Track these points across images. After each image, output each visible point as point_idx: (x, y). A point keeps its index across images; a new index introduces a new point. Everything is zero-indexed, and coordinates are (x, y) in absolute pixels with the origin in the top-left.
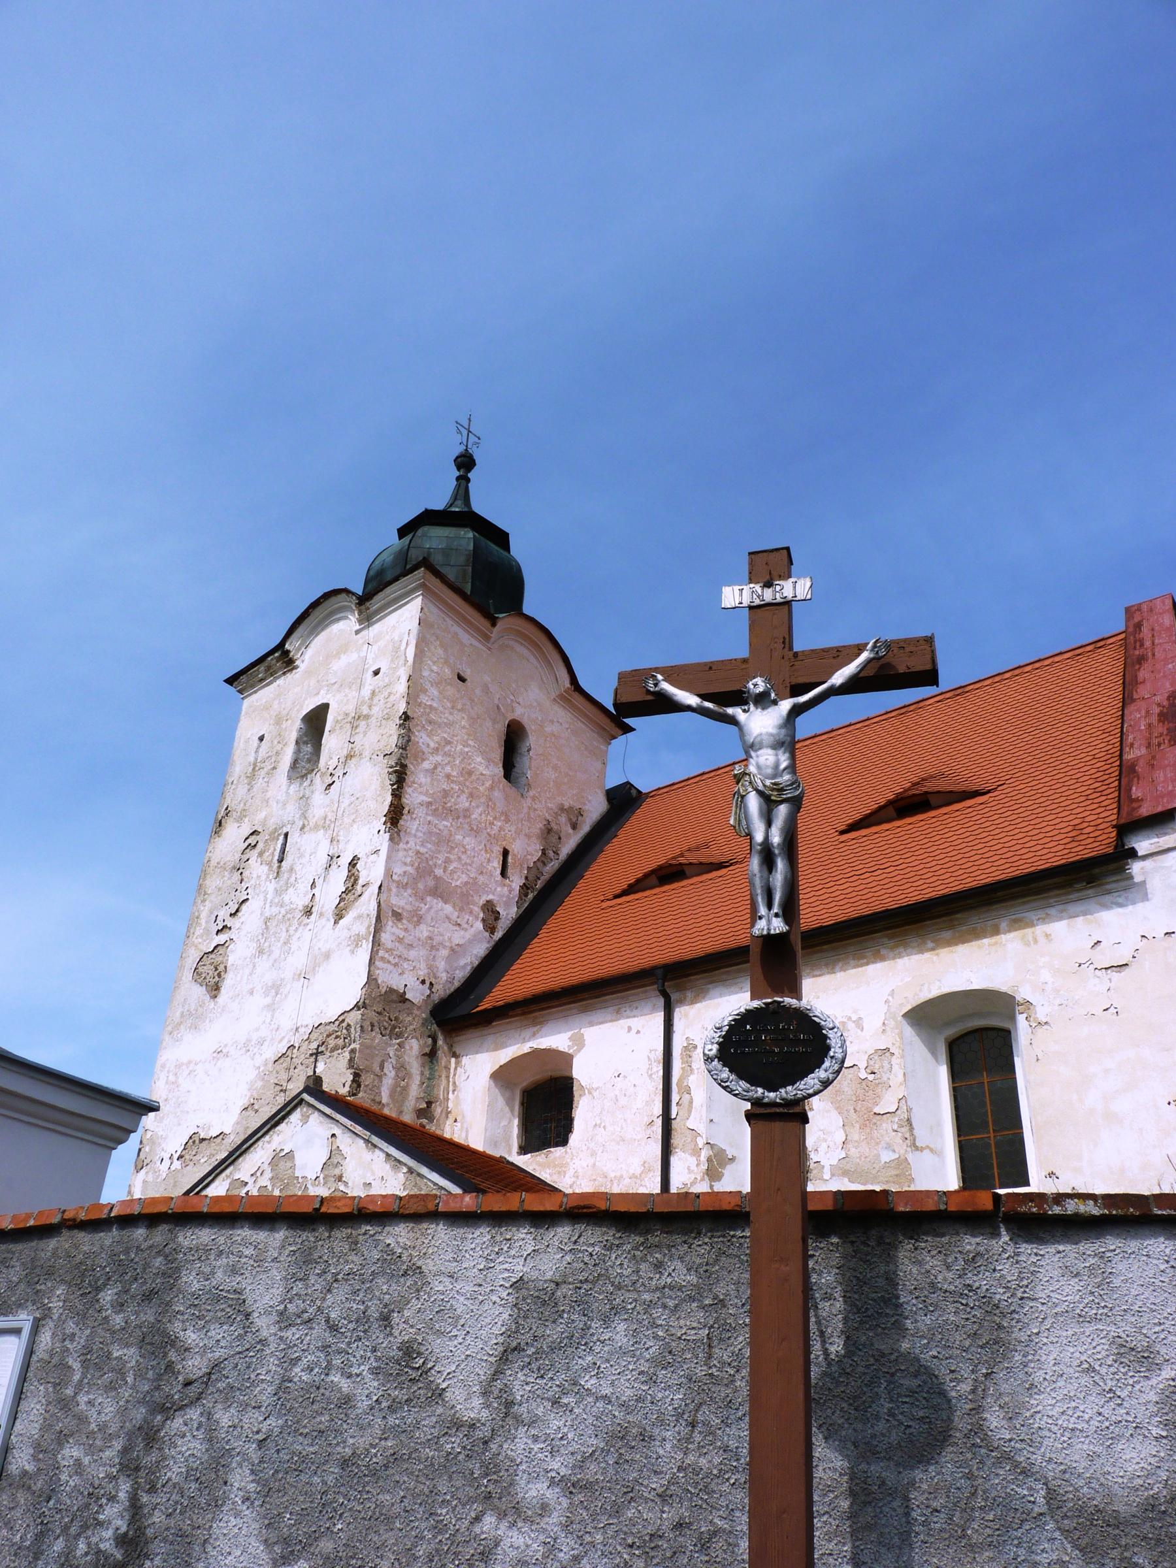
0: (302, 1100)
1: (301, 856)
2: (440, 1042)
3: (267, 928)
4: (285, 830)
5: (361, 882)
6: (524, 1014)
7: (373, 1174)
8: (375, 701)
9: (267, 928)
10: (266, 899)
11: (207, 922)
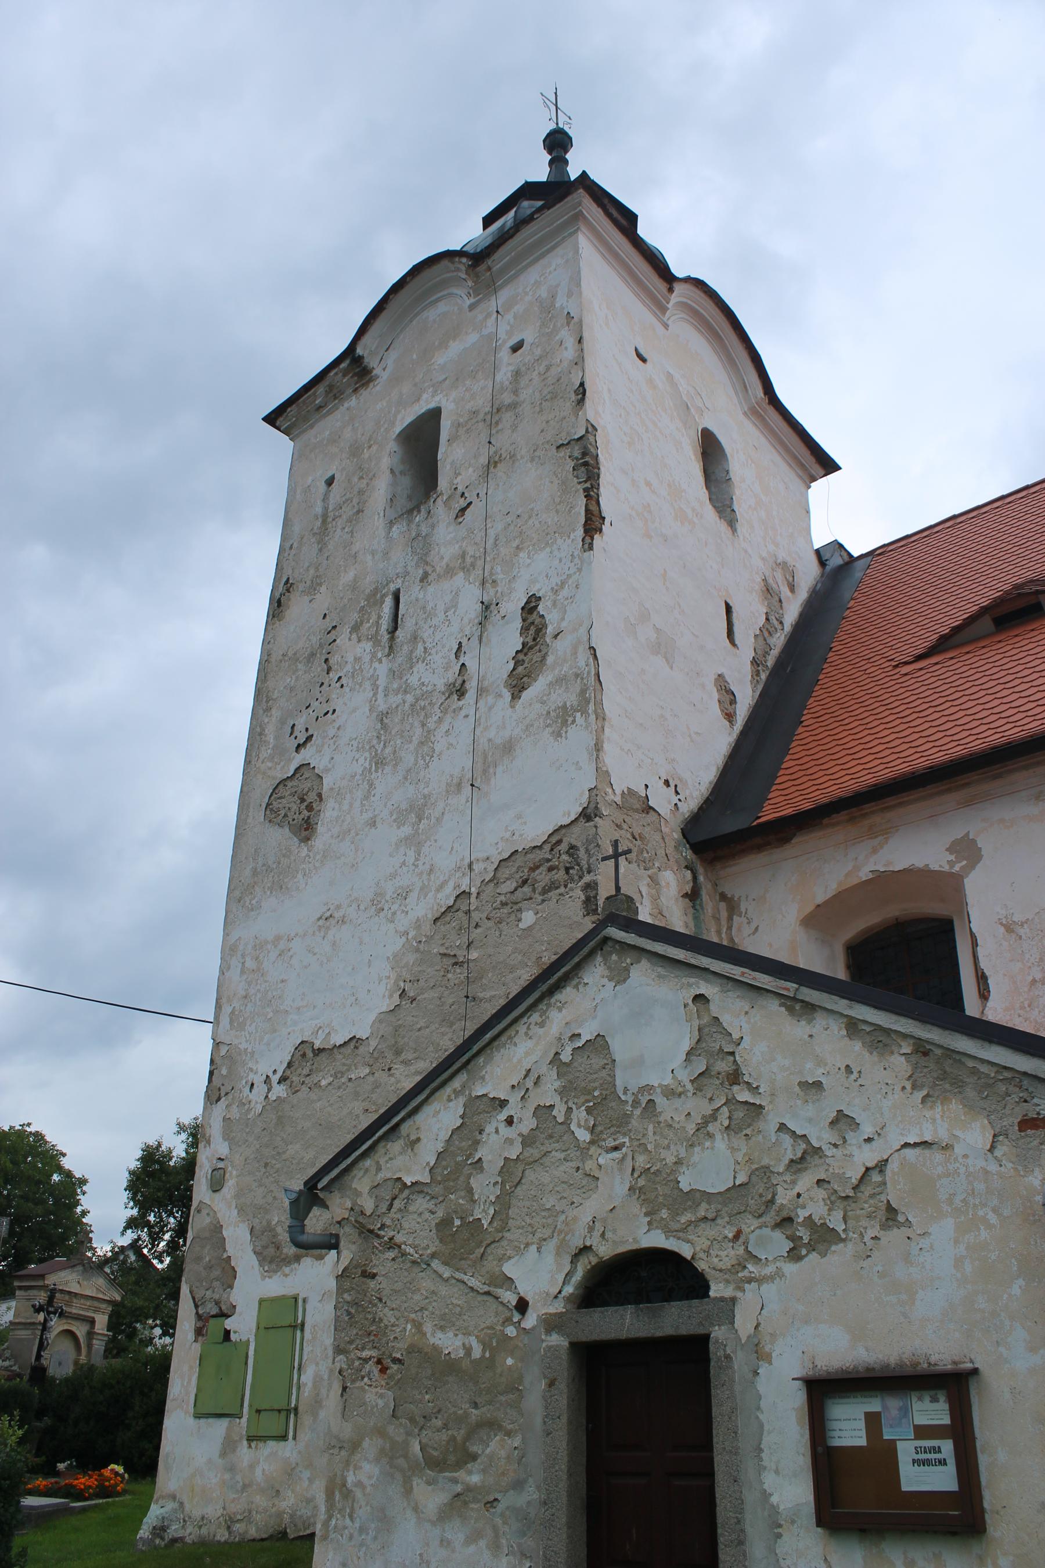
0: (606, 939)
1: (430, 616)
2: (701, 878)
3: (384, 726)
4: (392, 587)
5: (550, 630)
6: (852, 820)
7: (820, 1062)
8: (523, 382)
9: (384, 726)
10: (375, 687)
11: (276, 738)
